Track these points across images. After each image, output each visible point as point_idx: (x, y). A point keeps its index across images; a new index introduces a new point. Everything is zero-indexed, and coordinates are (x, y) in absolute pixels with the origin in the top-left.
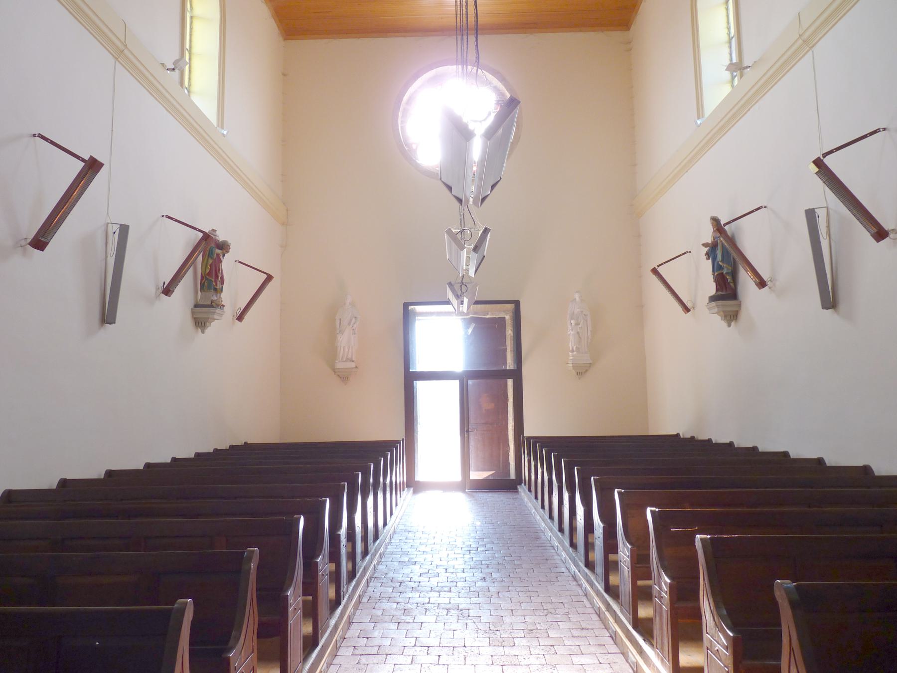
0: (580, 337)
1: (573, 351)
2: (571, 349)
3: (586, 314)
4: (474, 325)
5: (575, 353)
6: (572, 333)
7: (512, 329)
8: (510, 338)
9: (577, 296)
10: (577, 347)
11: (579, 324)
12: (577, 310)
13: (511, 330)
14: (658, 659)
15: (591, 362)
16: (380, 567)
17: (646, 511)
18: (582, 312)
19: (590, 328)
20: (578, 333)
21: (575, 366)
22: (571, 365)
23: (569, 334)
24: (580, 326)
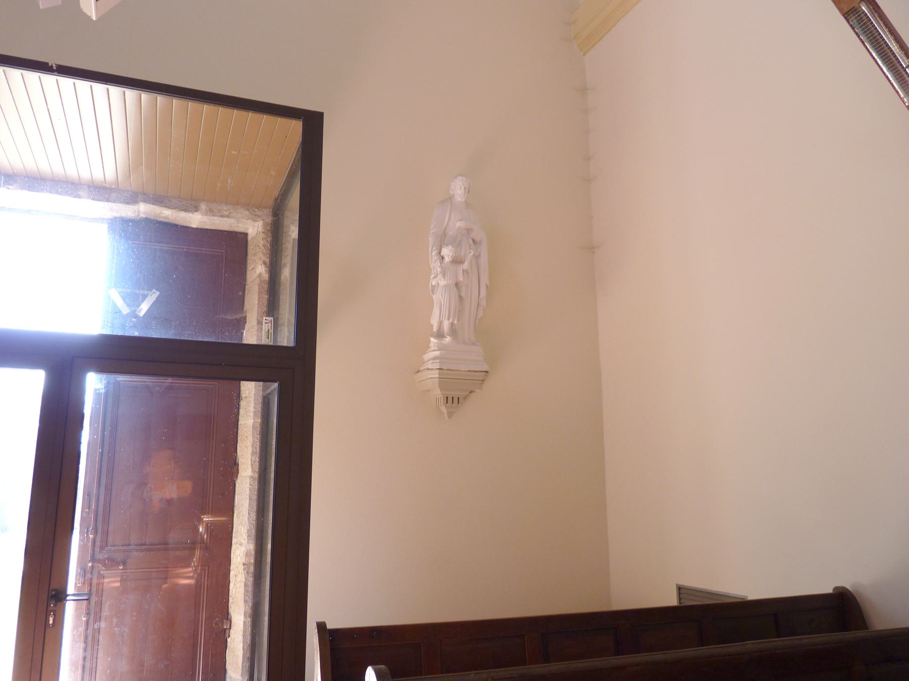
0: (460, 297)
1: (440, 335)
2: (435, 329)
3: (477, 239)
4: (158, 293)
5: (448, 339)
6: (443, 283)
7: (268, 261)
8: (260, 286)
9: (458, 189)
10: (452, 324)
11: (462, 262)
12: (457, 224)
13: (265, 263)
14: (231, 617)
15: (485, 367)
16: (148, 542)
17: (367, 669)
18: (469, 230)
19: (485, 280)
20: (457, 285)
21: (446, 377)
22: (436, 374)
23: (433, 287)
24: (466, 266)
